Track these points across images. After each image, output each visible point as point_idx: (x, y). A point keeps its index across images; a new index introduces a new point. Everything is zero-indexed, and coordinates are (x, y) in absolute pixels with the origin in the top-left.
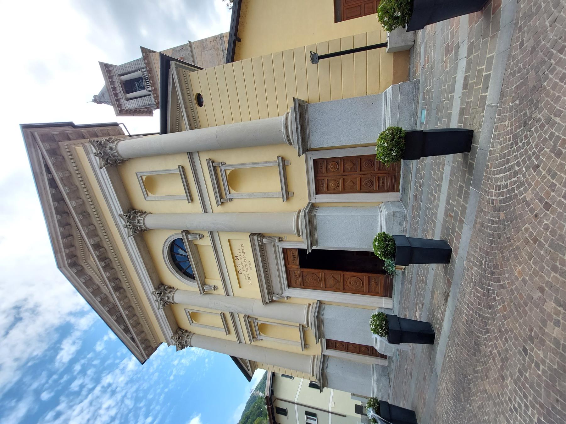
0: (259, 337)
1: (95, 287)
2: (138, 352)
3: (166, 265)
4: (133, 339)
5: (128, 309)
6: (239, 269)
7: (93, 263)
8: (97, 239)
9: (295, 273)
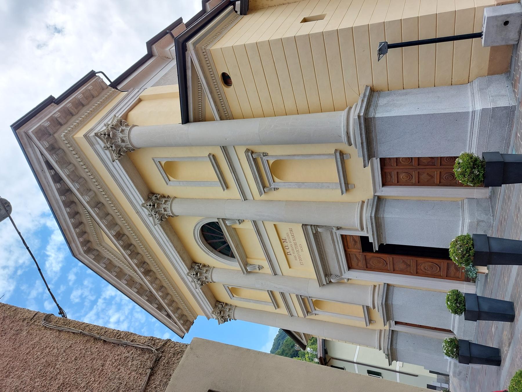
0: (316, 312)
1: (117, 270)
2: (176, 327)
3: (199, 245)
4: (168, 316)
5: (160, 290)
6: (287, 251)
7: (110, 243)
8: (117, 229)
9: (356, 256)
